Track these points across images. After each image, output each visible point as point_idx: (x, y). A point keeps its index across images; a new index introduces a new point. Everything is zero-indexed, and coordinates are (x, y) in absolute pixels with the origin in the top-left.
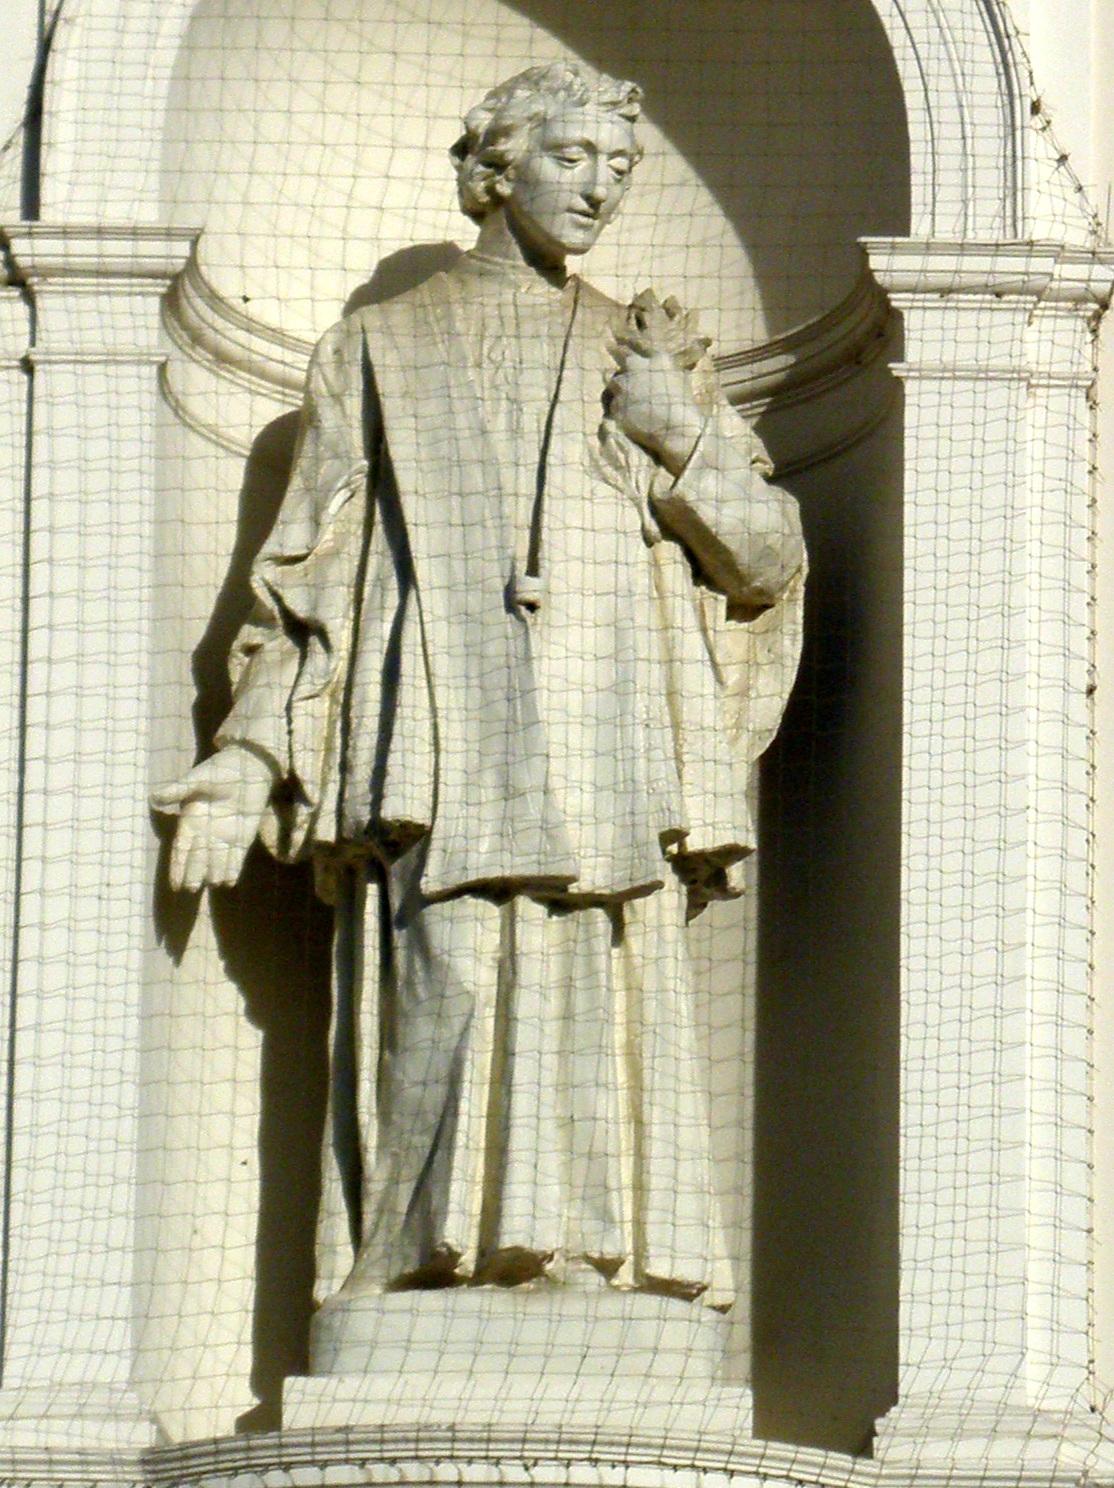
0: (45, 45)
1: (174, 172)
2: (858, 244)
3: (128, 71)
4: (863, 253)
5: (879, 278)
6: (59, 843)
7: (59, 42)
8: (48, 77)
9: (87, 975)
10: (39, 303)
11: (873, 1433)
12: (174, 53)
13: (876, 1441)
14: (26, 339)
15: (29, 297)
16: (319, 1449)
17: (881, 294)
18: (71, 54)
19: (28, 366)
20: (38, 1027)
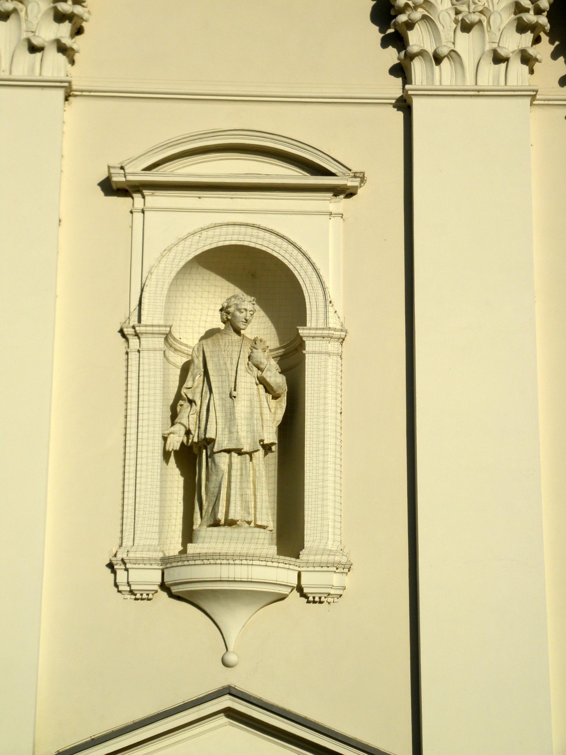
0: (142, 290)
4: (298, 330)
5: (301, 334)
6: (146, 386)
8: (143, 296)
13: (300, 556)
15: (139, 338)
19: (139, 351)
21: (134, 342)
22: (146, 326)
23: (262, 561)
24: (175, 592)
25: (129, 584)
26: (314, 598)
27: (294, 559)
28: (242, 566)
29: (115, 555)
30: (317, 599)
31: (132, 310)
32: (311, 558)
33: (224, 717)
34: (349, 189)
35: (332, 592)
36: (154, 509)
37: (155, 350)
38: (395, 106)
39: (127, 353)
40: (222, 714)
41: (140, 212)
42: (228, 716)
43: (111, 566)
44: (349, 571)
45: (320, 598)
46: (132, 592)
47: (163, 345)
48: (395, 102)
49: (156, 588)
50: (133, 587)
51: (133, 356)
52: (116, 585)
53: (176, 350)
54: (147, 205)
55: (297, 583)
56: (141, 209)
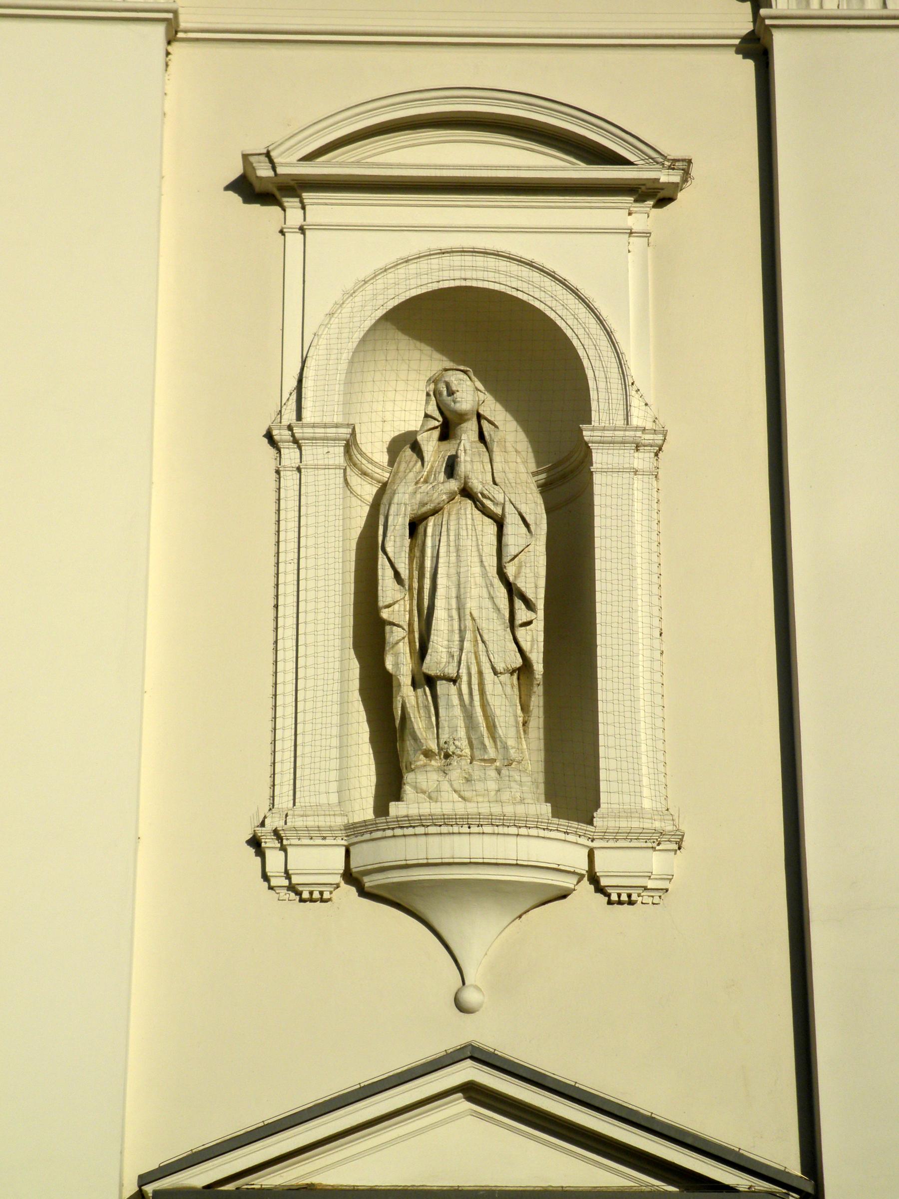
0: (304, 362)
1: (347, 403)
2: (580, 427)
3: (331, 372)
4: (581, 431)
6: (311, 595)
7: (308, 364)
8: (304, 375)
9: (322, 519)
10: (303, 448)
11: (593, 817)
12: (347, 364)
13: (594, 819)
14: (299, 461)
15: (300, 448)
16: (389, 824)
17: (586, 444)
18: (311, 368)
19: (299, 469)
20: (305, 678)
21: (290, 455)
22: (314, 426)
23: (497, 826)
24: (371, 887)
25: (288, 876)
26: (619, 895)
27: (584, 826)
28: (484, 835)
29: (263, 824)
30: (624, 898)
31: (286, 396)
32: (612, 824)
33: (463, 1100)
34: (662, 189)
35: (650, 884)
36: (328, 741)
37: (327, 467)
38: (739, 50)
39: (278, 472)
40: (460, 1095)
41: (299, 208)
42: (470, 1099)
43: (255, 843)
44: (679, 848)
45: (629, 896)
46: (292, 888)
47: (342, 459)
48: (740, 43)
49: (338, 879)
50: (295, 880)
51: (289, 479)
52: (265, 877)
53: (364, 474)
54: (309, 220)
55: (587, 869)
56: (298, 227)
